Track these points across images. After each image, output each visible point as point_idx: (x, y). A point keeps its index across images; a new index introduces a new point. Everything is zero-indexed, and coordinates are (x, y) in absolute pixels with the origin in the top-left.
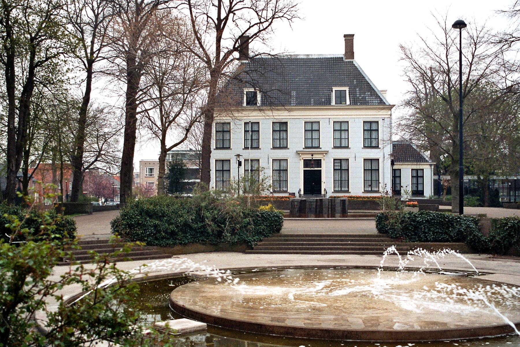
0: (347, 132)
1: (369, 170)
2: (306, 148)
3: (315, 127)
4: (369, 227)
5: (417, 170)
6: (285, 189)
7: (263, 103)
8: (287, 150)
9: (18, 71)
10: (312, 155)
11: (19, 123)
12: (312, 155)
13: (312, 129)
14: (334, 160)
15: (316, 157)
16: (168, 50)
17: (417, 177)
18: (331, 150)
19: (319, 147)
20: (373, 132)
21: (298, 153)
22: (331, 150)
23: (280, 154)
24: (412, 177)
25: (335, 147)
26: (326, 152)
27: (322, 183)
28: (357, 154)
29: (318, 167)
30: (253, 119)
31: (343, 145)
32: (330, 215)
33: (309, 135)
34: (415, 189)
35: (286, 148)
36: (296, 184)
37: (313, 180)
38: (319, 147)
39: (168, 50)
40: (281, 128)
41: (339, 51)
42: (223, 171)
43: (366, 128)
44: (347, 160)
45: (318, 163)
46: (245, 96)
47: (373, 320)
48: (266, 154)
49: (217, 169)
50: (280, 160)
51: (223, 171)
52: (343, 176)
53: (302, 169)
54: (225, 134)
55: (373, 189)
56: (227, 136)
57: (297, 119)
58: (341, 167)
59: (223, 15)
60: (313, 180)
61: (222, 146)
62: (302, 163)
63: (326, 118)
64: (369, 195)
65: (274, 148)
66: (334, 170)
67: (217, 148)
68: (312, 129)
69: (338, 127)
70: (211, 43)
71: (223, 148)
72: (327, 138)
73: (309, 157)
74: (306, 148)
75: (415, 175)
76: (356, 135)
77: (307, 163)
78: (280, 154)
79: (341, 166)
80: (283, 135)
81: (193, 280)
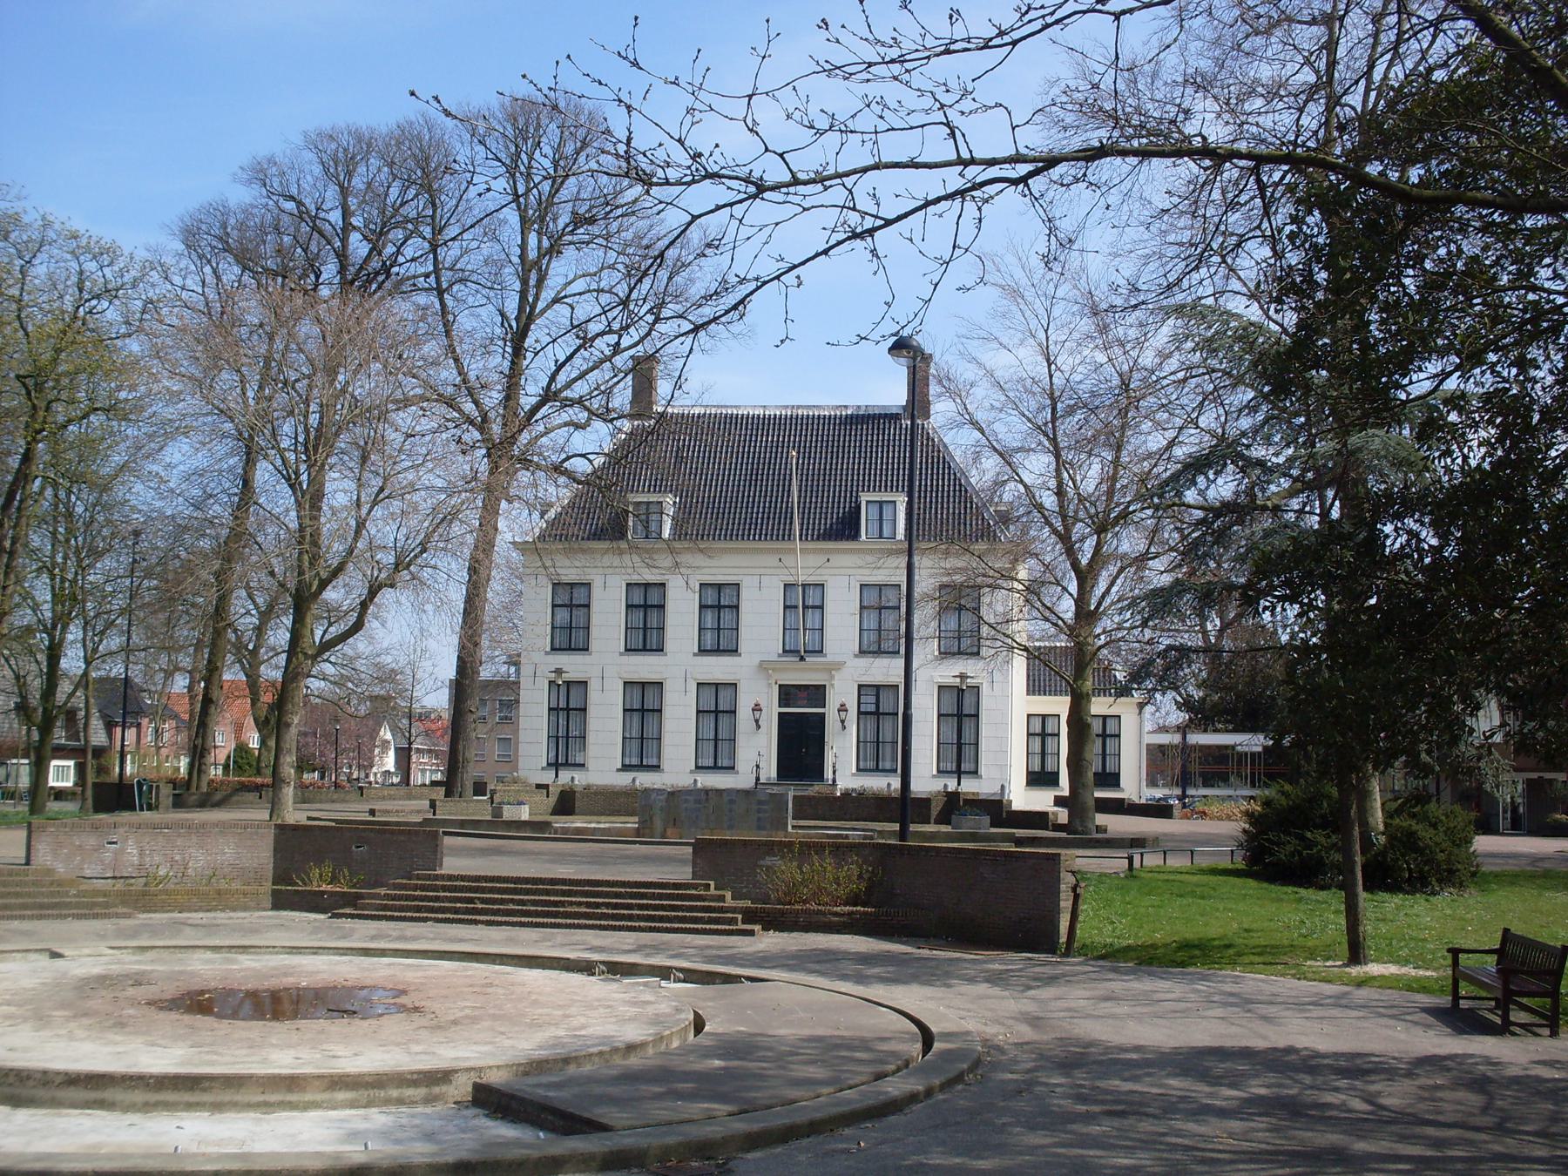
0: (818, 611)
3: (654, 599)
4: (669, 865)
7: (679, 532)
13: (804, 603)
17: (1044, 735)
23: (718, 668)
24: (1029, 735)
26: (838, 666)
33: (563, 615)
35: (734, 651)
36: (757, 753)
40: (720, 606)
41: (891, 392)
42: (717, 712)
44: (659, 685)
45: (817, 694)
48: (680, 667)
51: (717, 712)
56: (653, 621)
57: (762, 581)
59: (753, 285)
60: (801, 743)
63: (844, 576)
65: (702, 651)
68: (804, 603)
69: (638, 599)
71: (717, 651)
72: (842, 623)
75: (1038, 729)
76: (842, 623)
77: (788, 694)
78: (718, 668)
80: (812, 618)
81: (173, 1000)
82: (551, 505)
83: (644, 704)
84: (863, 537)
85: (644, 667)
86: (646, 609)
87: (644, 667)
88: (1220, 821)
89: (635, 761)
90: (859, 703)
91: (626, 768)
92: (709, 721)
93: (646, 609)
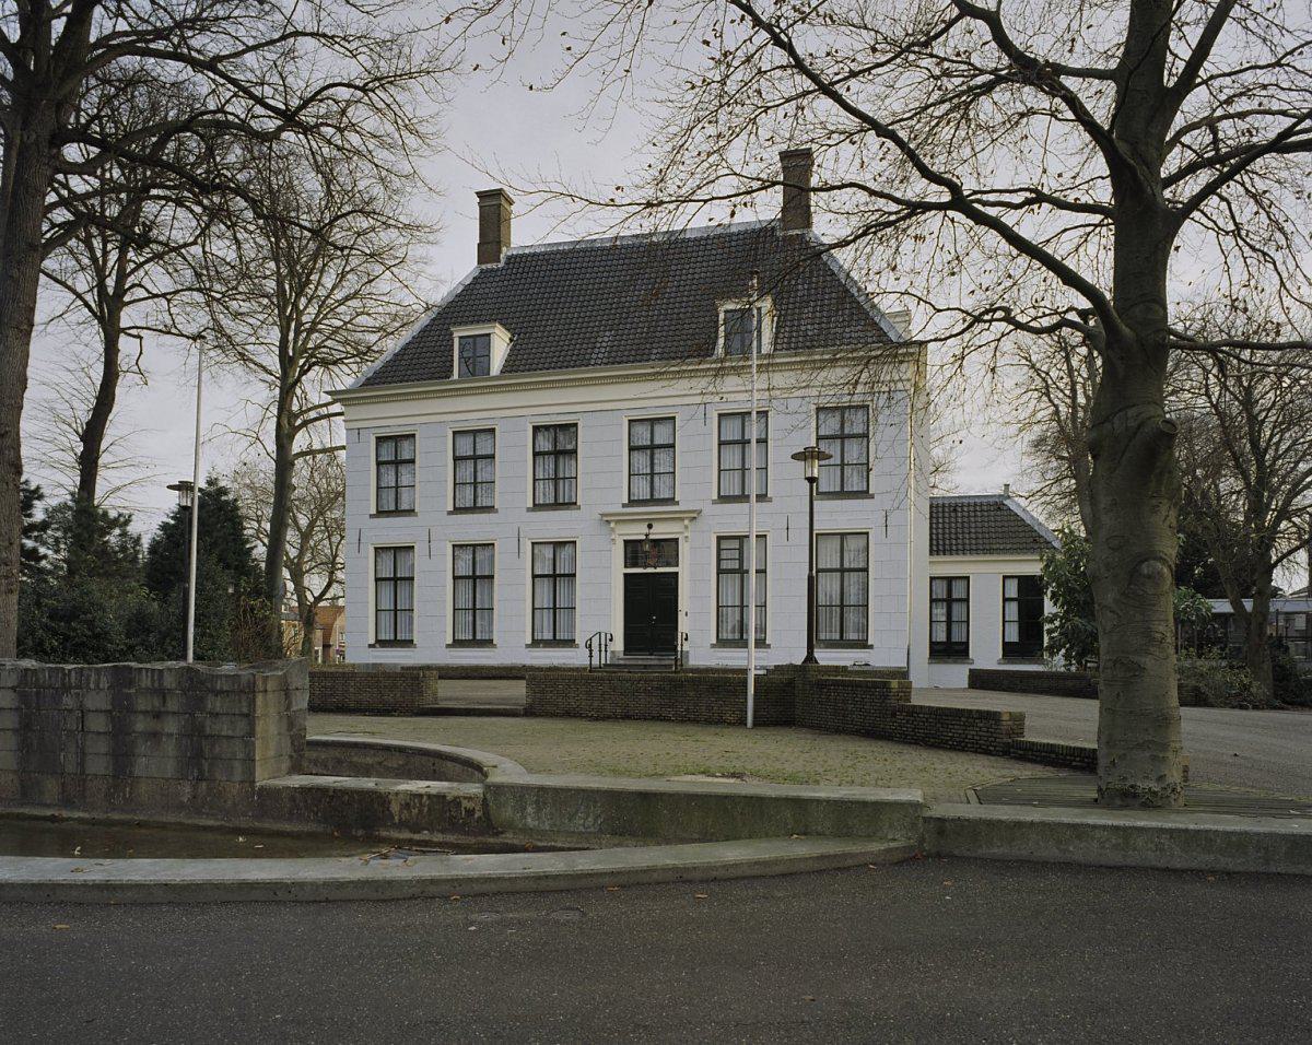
2: (632, 502)
3: (662, 436)
5: (950, 580)
9: (96, 245)
10: (650, 526)
11: (1208, 158)
12: (650, 526)
13: (651, 444)
14: (719, 539)
15: (661, 531)
16: (322, 124)
17: (949, 601)
18: (708, 509)
19: (671, 501)
20: (661, 456)
21: (607, 519)
22: (709, 509)
25: (723, 499)
26: (694, 516)
27: (681, 616)
28: (781, 523)
29: (668, 565)
30: (474, 421)
33: (642, 460)
34: (941, 636)
36: (601, 615)
37: (651, 604)
38: (671, 501)
39: (322, 124)
40: (557, 445)
44: (676, 540)
45: (666, 549)
46: (791, 233)
47: (655, 871)
48: (514, 525)
49: (538, 572)
50: (474, 546)
53: (618, 570)
54: (403, 469)
55: (478, 637)
60: (651, 604)
61: (552, 501)
64: (679, 637)
65: (381, 513)
68: (651, 444)
72: (696, 466)
73: (637, 532)
74: (632, 502)
77: (634, 551)
78: (555, 525)
82: (442, 282)
83: (475, 578)
84: (456, 376)
85: (473, 528)
86: (474, 454)
87: (473, 528)
88: (279, 663)
89: (548, 635)
90: (719, 560)
91: (457, 643)
92: (545, 587)
93: (474, 454)
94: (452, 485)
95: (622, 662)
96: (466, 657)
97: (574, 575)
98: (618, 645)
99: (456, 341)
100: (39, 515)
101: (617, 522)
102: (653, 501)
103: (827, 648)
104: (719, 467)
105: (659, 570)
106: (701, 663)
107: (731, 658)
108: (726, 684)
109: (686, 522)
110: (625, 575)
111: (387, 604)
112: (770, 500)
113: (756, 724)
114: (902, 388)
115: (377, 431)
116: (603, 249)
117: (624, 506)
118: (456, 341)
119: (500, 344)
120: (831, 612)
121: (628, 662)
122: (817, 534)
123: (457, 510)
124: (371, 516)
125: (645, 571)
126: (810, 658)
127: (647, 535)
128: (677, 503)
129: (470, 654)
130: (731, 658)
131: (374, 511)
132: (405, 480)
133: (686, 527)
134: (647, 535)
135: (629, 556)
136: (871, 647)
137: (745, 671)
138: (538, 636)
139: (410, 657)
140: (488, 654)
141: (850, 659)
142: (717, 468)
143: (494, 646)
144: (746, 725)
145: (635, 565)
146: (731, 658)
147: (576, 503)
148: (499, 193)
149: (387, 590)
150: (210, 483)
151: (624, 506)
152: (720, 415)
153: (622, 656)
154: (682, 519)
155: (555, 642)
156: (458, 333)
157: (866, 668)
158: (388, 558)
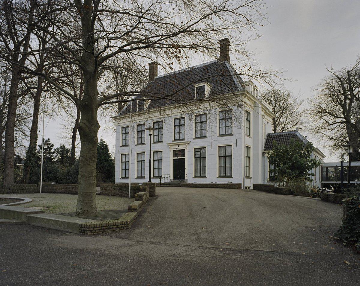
1: (223, 156)
2: (175, 140)
6: (229, 175)
8: (144, 145)
10: (179, 146)
12: (179, 146)
14: (195, 149)
15: (181, 147)
19: (184, 139)
21: (170, 145)
22: (193, 141)
31: (181, 138)
32: (34, 186)
36: (168, 171)
37: (179, 166)
38: (184, 139)
43: (176, 124)
45: (183, 152)
52: (157, 165)
53: (171, 158)
55: (202, 175)
58: (200, 156)
61: (158, 141)
62: (172, 153)
66: (195, 158)
67: (154, 142)
69: (177, 124)
70: (141, 45)
73: (175, 148)
74: (175, 140)
77: (176, 153)
79: (200, 154)
83: (225, 158)
89: (199, 175)
94: (218, 128)
95: (172, 182)
96: (139, 181)
97: (231, 156)
98: (172, 178)
99: (195, 88)
100: (52, 151)
101: (171, 145)
102: (180, 140)
103: (221, 178)
104: (219, 126)
105: (181, 158)
106: (190, 182)
107: (125, 181)
108: (124, 187)
109: (186, 145)
110: (174, 159)
111: (198, 165)
112: (233, 135)
113: (42, 193)
114: (163, 117)
115: (122, 126)
116: (177, 73)
117: (173, 141)
118: (195, 88)
119: (208, 89)
120: (223, 168)
121: (174, 182)
122: (154, 152)
123: (138, 144)
124: (121, 147)
125: (180, 158)
126: (150, 181)
127: (177, 149)
128: (185, 140)
129: (138, 180)
130: (197, 181)
131: (121, 146)
132: (143, 136)
133: (186, 146)
134: (177, 149)
135: (175, 154)
136: (232, 178)
137: (128, 184)
138: (155, 176)
139: (205, 181)
140: (205, 180)
141: (226, 181)
142: (218, 127)
143: (206, 178)
144: (128, 197)
145: (176, 157)
146: (197, 181)
147: (206, 136)
148: (226, 40)
149: (124, 164)
150: (101, 140)
151: (173, 141)
152: (122, 128)
153: (173, 180)
154: (185, 144)
155: (226, 177)
156: (197, 85)
157: (231, 184)
158: (124, 157)
